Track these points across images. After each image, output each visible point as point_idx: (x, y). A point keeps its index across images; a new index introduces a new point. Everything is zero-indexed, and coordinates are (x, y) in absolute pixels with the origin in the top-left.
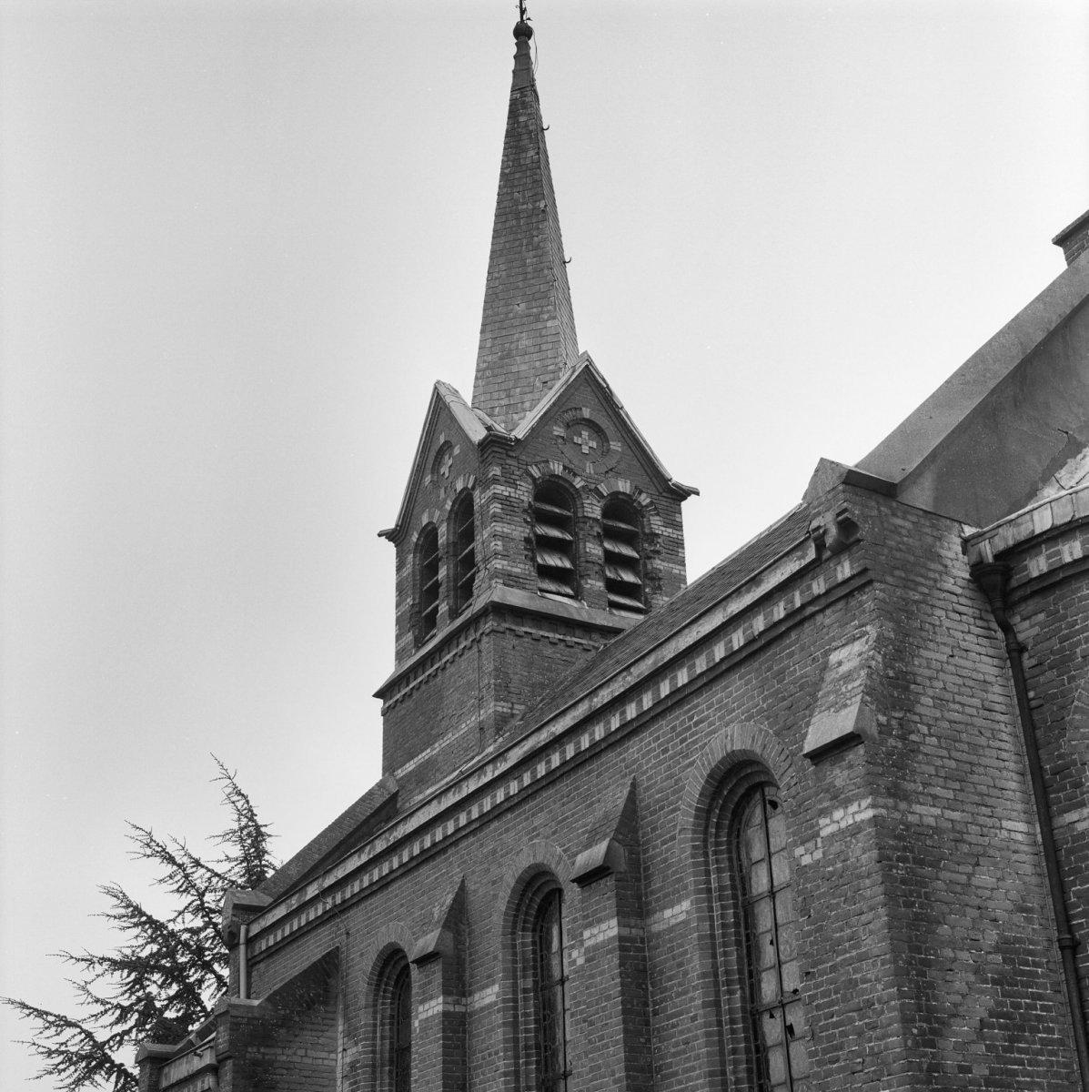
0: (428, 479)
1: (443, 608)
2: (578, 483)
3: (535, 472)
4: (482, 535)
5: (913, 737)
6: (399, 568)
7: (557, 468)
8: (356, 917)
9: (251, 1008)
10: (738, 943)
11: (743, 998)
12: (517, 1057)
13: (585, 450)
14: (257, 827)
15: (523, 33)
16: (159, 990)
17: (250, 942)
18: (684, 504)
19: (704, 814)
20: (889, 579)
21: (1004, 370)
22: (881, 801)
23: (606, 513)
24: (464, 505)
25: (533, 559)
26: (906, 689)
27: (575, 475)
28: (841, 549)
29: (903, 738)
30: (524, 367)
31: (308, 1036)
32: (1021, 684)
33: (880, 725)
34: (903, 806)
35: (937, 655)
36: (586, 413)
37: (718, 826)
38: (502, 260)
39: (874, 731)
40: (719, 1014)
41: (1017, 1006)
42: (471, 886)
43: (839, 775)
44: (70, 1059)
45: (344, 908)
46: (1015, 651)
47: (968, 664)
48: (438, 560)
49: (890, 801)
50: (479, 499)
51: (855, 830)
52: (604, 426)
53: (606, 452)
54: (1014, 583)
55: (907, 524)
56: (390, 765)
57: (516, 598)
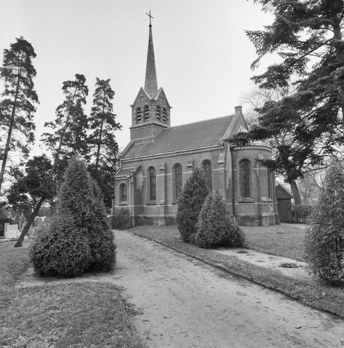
0: (139, 100)
7: (159, 104)
15: (150, 26)
32: (232, 158)
43: (221, 165)
46: (232, 155)
51: (222, 170)
57: (155, 122)
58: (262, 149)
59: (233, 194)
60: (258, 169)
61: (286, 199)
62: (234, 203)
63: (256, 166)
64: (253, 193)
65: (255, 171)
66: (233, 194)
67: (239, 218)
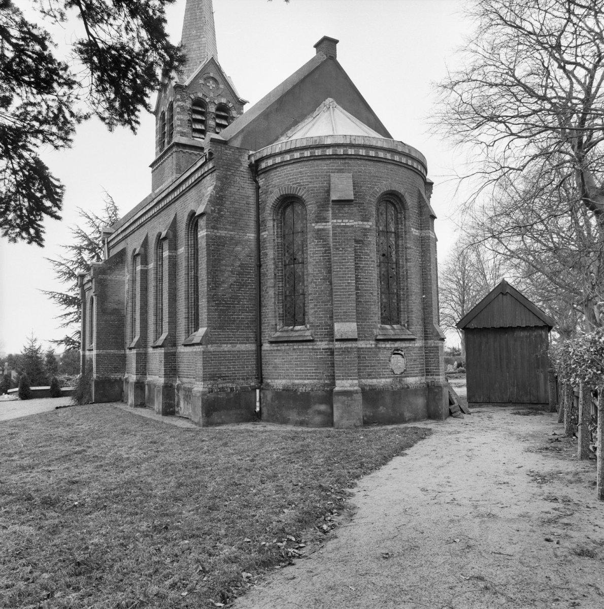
1: (166, 141)
2: (207, 100)
3: (192, 97)
4: (175, 118)
5: (222, 213)
6: (157, 124)
7: (200, 95)
8: (129, 240)
9: (99, 265)
10: (194, 259)
11: (194, 273)
12: (157, 282)
13: (211, 88)
14: (115, 207)
16: (86, 255)
17: (108, 243)
18: (244, 106)
19: (188, 225)
20: (222, 169)
21: (273, 100)
22: (209, 230)
23: (217, 110)
24: (171, 105)
25: (191, 126)
26: (222, 200)
27: (206, 97)
28: (210, 159)
29: (218, 213)
30: (194, 56)
31: (117, 272)
33: (211, 210)
34: (215, 231)
35: (233, 190)
36: (211, 75)
37: (191, 228)
38: (189, 13)
39: (209, 211)
40: (188, 276)
41: (243, 280)
42: (149, 235)
44: (65, 274)
45: (126, 237)
47: (244, 192)
48: (165, 124)
49: (212, 230)
50: (175, 105)
52: (217, 79)
53: (218, 88)
54: (259, 169)
55: (230, 152)
56: (153, 190)
57: (184, 140)
58: (346, 157)
59: (157, 311)
60: (329, 226)
61: (527, 328)
62: (260, 345)
63: (324, 214)
64: (313, 312)
65: (320, 235)
66: (157, 311)
67: (269, 395)
